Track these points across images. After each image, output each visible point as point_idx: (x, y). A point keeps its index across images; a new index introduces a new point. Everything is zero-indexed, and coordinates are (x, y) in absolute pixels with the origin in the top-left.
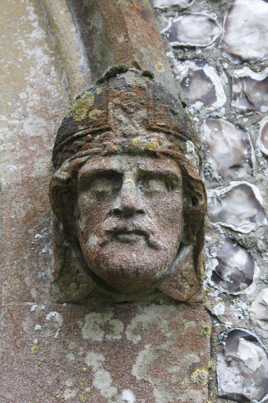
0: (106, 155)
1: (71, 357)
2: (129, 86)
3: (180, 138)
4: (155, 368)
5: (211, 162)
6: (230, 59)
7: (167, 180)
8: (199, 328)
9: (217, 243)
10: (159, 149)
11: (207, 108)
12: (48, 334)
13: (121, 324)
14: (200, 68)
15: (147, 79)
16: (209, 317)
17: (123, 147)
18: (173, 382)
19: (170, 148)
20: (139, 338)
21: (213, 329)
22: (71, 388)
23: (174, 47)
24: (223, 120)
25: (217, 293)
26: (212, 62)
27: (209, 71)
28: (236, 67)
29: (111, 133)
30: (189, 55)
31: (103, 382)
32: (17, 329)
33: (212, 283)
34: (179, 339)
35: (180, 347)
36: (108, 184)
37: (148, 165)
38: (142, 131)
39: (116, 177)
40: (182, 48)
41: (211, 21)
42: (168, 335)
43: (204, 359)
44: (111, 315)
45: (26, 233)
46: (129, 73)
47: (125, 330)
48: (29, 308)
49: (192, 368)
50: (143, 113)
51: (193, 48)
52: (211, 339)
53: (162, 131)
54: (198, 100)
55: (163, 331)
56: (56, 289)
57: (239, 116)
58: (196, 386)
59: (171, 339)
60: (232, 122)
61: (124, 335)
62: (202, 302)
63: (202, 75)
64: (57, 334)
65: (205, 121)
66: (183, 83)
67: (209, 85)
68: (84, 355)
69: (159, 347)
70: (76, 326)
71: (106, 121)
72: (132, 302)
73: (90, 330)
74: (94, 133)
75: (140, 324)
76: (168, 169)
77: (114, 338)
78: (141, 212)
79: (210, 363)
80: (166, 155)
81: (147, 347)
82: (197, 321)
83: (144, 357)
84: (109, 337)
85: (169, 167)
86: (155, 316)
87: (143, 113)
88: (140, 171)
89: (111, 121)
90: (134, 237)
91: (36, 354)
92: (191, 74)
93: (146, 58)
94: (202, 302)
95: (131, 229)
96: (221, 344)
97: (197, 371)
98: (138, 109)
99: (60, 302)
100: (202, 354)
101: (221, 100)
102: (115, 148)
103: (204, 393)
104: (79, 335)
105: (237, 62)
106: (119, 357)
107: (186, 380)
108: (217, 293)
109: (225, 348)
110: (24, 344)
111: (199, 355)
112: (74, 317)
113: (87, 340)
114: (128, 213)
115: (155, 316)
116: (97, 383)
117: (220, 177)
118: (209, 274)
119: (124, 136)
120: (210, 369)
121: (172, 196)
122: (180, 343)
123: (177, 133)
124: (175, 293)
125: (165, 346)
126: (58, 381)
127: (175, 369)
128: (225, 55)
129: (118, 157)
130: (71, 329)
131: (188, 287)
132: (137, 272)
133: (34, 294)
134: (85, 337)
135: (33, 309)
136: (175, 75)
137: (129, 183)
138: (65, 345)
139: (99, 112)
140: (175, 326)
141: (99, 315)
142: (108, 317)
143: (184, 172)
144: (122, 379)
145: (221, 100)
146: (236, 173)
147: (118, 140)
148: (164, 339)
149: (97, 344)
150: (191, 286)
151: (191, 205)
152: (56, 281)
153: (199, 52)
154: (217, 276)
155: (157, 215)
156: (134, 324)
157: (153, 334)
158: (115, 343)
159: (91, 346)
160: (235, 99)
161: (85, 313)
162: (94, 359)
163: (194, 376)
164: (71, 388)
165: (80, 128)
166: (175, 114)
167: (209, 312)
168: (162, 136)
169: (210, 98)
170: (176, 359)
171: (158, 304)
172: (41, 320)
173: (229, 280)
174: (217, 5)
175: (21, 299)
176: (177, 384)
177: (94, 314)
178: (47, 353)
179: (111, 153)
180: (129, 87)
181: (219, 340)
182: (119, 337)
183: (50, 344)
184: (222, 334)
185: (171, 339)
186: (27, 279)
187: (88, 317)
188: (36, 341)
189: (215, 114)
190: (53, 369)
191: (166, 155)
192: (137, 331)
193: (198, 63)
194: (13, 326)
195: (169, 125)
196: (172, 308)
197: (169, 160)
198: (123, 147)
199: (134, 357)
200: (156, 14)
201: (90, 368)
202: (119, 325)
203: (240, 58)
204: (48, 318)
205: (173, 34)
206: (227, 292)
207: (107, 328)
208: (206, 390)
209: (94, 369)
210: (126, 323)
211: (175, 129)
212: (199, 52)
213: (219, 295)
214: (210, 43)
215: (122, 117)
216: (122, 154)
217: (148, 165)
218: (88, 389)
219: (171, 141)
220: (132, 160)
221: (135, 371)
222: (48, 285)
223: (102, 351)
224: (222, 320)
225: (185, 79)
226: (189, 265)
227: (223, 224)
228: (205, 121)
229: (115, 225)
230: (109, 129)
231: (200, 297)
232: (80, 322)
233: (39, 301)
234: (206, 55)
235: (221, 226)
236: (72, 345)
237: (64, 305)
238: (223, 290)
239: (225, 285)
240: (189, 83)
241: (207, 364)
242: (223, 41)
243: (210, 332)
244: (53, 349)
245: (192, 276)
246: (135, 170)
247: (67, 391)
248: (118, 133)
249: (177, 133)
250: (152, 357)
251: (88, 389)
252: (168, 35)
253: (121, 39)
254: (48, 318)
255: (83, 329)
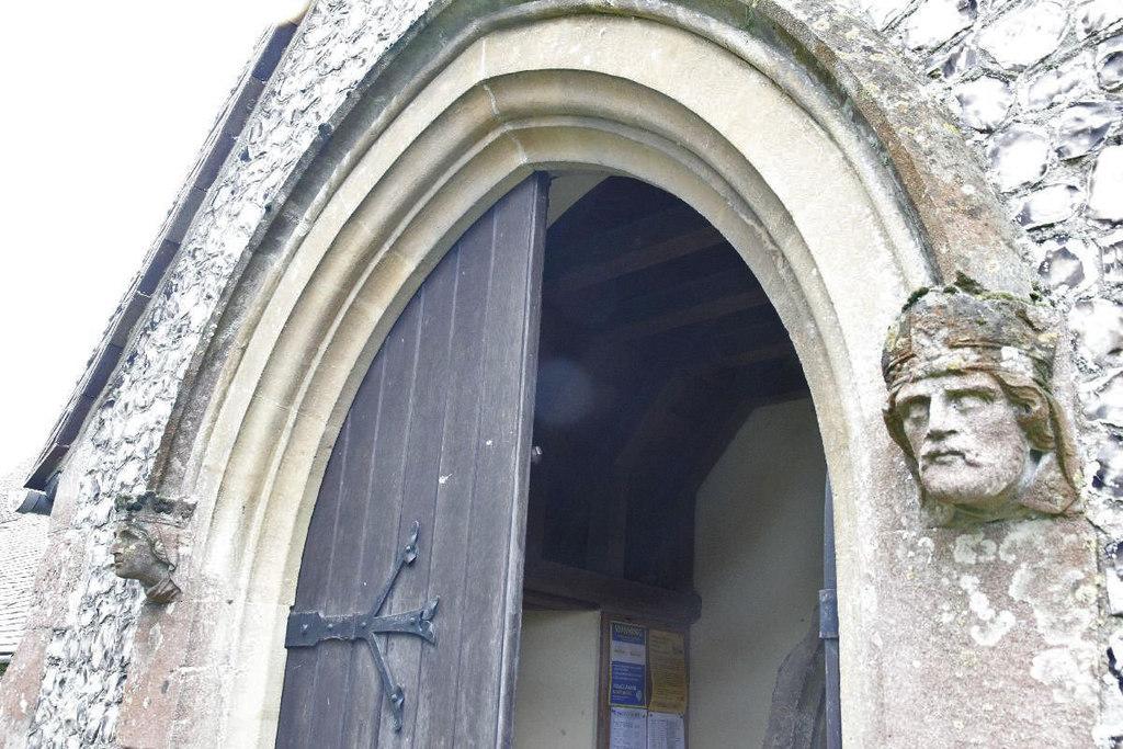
0: (913, 382)
1: (945, 581)
2: (930, 308)
3: (993, 348)
4: (1033, 588)
5: (1082, 351)
6: (1098, 225)
7: (984, 395)
8: (1080, 542)
9: (1098, 443)
10: (964, 364)
11: (1075, 290)
12: (922, 559)
13: (993, 544)
14: (1062, 247)
15: (948, 295)
16: (1091, 528)
17: (926, 372)
18: (1056, 601)
19: (978, 361)
20: (1013, 557)
21: (1098, 542)
22: (949, 612)
23: (1029, 231)
24: (1096, 299)
25: (1100, 500)
26: (1078, 235)
27: (1071, 246)
28: (1106, 233)
29: (915, 359)
30: (1048, 233)
31: (980, 603)
32: (892, 556)
33: (1094, 490)
34: (1059, 556)
35: (1060, 563)
36: (921, 409)
37: (954, 383)
38: (945, 350)
39: (924, 401)
40: (1038, 228)
41: (1072, 188)
42: (1046, 551)
43: (1089, 575)
44: (982, 535)
45: (892, 463)
46: (930, 294)
47: (998, 550)
48: (901, 536)
49: (1076, 586)
50: (944, 332)
51: (1052, 225)
52: (1097, 553)
53: (967, 346)
54: (1062, 283)
55: (1039, 548)
56: (925, 514)
57: (1115, 291)
58: (1083, 604)
59: (1049, 556)
60: (1108, 298)
61: (996, 554)
62: (1082, 513)
63: (1065, 253)
64: (930, 558)
65: (1073, 306)
66: (1041, 270)
67: (1075, 263)
68: (958, 579)
69: (1035, 566)
70: (948, 550)
71: (910, 348)
72: (1003, 520)
73: (962, 551)
74: (902, 362)
75: (1014, 543)
76: (977, 384)
77: (988, 559)
78: (953, 432)
79: (1098, 579)
80: (974, 369)
81: (1024, 565)
82: (1078, 535)
83: (1021, 577)
84: (982, 559)
85: (981, 381)
86: (1029, 533)
87: (944, 332)
88: (948, 392)
89: (915, 346)
90: (949, 458)
91: (912, 580)
92: (1050, 256)
93: (974, 263)
94: (1082, 513)
95: (943, 450)
96: (1111, 558)
97: (1082, 589)
98: (938, 329)
99: (929, 527)
100: (1086, 569)
101: (1092, 273)
102: (920, 373)
103: (1092, 612)
104: (952, 559)
105: (1107, 227)
106: (994, 577)
107: (1070, 598)
108: (1100, 500)
109: (1115, 561)
110: (900, 572)
111: (1083, 571)
112: (945, 541)
113: (960, 564)
114: (937, 436)
115: (1029, 533)
116: (974, 606)
117: (1097, 367)
118: (1090, 480)
119: (928, 359)
120: (1099, 586)
121: (992, 408)
122: (1060, 559)
123: (986, 343)
124: (1046, 506)
125: (1042, 564)
126: (936, 606)
127: (1057, 588)
128: (1091, 222)
129: (924, 381)
130: (943, 554)
131: (1061, 497)
132: (957, 491)
133: (904, 521)
134: (958, 560)
135: (905, 537)
136: (1031, 262)
137: (937, 405)
138: (938, 569)
139: (903, 340)
140: (1054, 542)
141: (970, 536)
142: (979, 538)
143: (1001, 382)
144: (999, 599)
145: (1092, 273)
146: (1117, 358)
147: (922, 365)
148: (1041, 556)
149: (970, 566)
150: (1065, 496)
151: (1024, 413)
152: (922, 506)
153: (1058, 228)
154: (1098, 482)
155: (975, 431)
156: (1006, 544)
157: (1029, 551)
158: (989, 564)
159: (965, 569)
160: (1108, 271)
161: (955, 536)
162: (969, 582)
163: (1079, 594)
164: (949, 612)
165: (892, 358)
166: (982, 324)
167: (1091, 522)
168: (967, 351)
169: (1075, 279)
170: (1056, 577)
171: (1030, 519)
172: (913, 547)
173: (1113, 485)
174: (1077, 167)
175: (893, 528)
176: (1060, 603)
177: (964, 536)
178: (922, 579)
179: (917, 379)
180: (929, 309)
181: (1107, 553)
182: (992, 558)
183: (924, 570)
184: (1111, 546)
185: (1049, 556)
186: (897, 509)
187: (958, 540)
188: (910, 568)
189: (1085, 295)
190: (930, 593)
191: (974, 369)
192: (1012, 549)
193: (1060, 240)
194: (887, 554)
195: (974, 338)
196: (1048, 522)
197: (978, 374)
198: (926, 372)
199: (1009, 578)
200: (1004, 201)
201: (966, 592)
202: (991, 546)
203: (1109, 221)
204: (920, 544)
205: (1025, 218)
206: (1112, 497)
207: (979, 549)
208: (1095, 608)
209: (969, 592)
210: (999, 540)
211: (983, 339)
212: (1058, 228)
213: (1104, 503)
214: (1067, 213)
215: (925, 341)
216: (925, 378)
217: (954, 383)
218: (965, 613)
219: (979, 353)
220: (937, 382)
221: (1013, 592)
222: (917, 511)
223: (976, 573)
224: (1105, 529)
225: (1042, 264)
226: (1055, 474)
227: (1103, 421)
228: (1073, 306)
229: (928, 450)
230: (913, 356)
231: (1078, 507)
232: (951, 546)
233: (910, 528)
234: (1067, 230)
235: (1103, 424)
236: (945, 570)
237: (935, 529)
238: (1108, 497)
239: (1110, 491)
240: (1049, 267)
241: (1094, 580)
242: (1088, 207)
243: (1094, 544)
244: (928, 574)
245: (1064, 484)
246: (941, 391)
247: (945, 614)
248: (922, 357)
249: (986, 343)
250: (1030, 576)
251: (965, 613)
252: (1020, 220)
253: (944, 250)
254: (920, 544)
255: (955, 553)
